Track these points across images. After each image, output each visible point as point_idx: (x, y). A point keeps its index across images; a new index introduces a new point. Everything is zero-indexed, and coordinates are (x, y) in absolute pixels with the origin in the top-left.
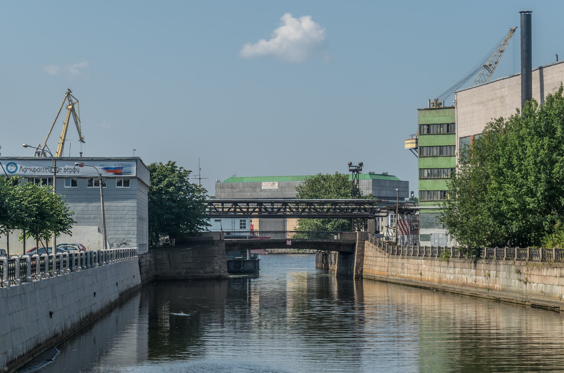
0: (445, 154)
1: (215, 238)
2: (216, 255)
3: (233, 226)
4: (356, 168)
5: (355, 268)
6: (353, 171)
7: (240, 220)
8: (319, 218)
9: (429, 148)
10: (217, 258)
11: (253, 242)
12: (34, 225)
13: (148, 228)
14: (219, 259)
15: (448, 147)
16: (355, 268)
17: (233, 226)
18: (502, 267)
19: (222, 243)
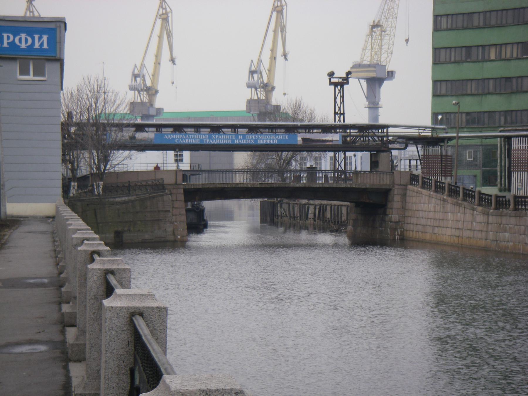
0: (474, 57)
1: (166, 182)
2: (169, 209)
3: (165, 159)
4: (341, 80)
5: (157, 194)
6: (336, 85)
7: (332, 157)
8: (256, 151)
9: (448, 50)
10: (170, 214)
11: (227, 188)
12: (514, 352)
13: (142, 170)
14: (173, 215)
15: (480, 48)
16: (157, 194)
17: (165, 159)
18: (415, 207)
19: (179, 188)
